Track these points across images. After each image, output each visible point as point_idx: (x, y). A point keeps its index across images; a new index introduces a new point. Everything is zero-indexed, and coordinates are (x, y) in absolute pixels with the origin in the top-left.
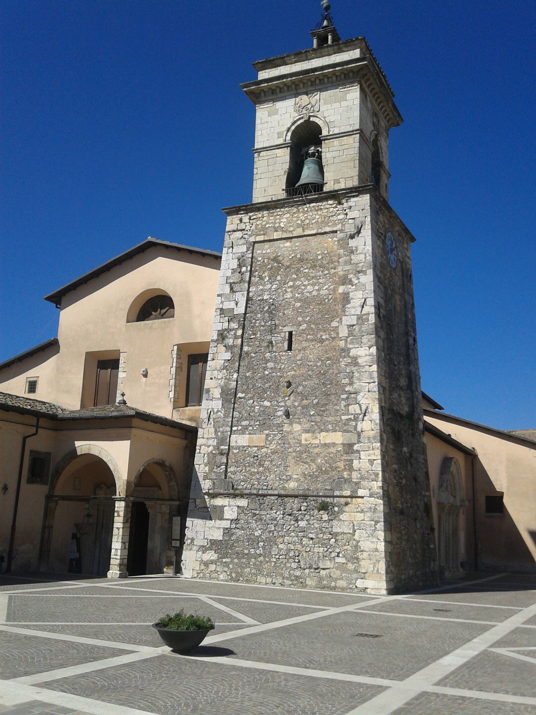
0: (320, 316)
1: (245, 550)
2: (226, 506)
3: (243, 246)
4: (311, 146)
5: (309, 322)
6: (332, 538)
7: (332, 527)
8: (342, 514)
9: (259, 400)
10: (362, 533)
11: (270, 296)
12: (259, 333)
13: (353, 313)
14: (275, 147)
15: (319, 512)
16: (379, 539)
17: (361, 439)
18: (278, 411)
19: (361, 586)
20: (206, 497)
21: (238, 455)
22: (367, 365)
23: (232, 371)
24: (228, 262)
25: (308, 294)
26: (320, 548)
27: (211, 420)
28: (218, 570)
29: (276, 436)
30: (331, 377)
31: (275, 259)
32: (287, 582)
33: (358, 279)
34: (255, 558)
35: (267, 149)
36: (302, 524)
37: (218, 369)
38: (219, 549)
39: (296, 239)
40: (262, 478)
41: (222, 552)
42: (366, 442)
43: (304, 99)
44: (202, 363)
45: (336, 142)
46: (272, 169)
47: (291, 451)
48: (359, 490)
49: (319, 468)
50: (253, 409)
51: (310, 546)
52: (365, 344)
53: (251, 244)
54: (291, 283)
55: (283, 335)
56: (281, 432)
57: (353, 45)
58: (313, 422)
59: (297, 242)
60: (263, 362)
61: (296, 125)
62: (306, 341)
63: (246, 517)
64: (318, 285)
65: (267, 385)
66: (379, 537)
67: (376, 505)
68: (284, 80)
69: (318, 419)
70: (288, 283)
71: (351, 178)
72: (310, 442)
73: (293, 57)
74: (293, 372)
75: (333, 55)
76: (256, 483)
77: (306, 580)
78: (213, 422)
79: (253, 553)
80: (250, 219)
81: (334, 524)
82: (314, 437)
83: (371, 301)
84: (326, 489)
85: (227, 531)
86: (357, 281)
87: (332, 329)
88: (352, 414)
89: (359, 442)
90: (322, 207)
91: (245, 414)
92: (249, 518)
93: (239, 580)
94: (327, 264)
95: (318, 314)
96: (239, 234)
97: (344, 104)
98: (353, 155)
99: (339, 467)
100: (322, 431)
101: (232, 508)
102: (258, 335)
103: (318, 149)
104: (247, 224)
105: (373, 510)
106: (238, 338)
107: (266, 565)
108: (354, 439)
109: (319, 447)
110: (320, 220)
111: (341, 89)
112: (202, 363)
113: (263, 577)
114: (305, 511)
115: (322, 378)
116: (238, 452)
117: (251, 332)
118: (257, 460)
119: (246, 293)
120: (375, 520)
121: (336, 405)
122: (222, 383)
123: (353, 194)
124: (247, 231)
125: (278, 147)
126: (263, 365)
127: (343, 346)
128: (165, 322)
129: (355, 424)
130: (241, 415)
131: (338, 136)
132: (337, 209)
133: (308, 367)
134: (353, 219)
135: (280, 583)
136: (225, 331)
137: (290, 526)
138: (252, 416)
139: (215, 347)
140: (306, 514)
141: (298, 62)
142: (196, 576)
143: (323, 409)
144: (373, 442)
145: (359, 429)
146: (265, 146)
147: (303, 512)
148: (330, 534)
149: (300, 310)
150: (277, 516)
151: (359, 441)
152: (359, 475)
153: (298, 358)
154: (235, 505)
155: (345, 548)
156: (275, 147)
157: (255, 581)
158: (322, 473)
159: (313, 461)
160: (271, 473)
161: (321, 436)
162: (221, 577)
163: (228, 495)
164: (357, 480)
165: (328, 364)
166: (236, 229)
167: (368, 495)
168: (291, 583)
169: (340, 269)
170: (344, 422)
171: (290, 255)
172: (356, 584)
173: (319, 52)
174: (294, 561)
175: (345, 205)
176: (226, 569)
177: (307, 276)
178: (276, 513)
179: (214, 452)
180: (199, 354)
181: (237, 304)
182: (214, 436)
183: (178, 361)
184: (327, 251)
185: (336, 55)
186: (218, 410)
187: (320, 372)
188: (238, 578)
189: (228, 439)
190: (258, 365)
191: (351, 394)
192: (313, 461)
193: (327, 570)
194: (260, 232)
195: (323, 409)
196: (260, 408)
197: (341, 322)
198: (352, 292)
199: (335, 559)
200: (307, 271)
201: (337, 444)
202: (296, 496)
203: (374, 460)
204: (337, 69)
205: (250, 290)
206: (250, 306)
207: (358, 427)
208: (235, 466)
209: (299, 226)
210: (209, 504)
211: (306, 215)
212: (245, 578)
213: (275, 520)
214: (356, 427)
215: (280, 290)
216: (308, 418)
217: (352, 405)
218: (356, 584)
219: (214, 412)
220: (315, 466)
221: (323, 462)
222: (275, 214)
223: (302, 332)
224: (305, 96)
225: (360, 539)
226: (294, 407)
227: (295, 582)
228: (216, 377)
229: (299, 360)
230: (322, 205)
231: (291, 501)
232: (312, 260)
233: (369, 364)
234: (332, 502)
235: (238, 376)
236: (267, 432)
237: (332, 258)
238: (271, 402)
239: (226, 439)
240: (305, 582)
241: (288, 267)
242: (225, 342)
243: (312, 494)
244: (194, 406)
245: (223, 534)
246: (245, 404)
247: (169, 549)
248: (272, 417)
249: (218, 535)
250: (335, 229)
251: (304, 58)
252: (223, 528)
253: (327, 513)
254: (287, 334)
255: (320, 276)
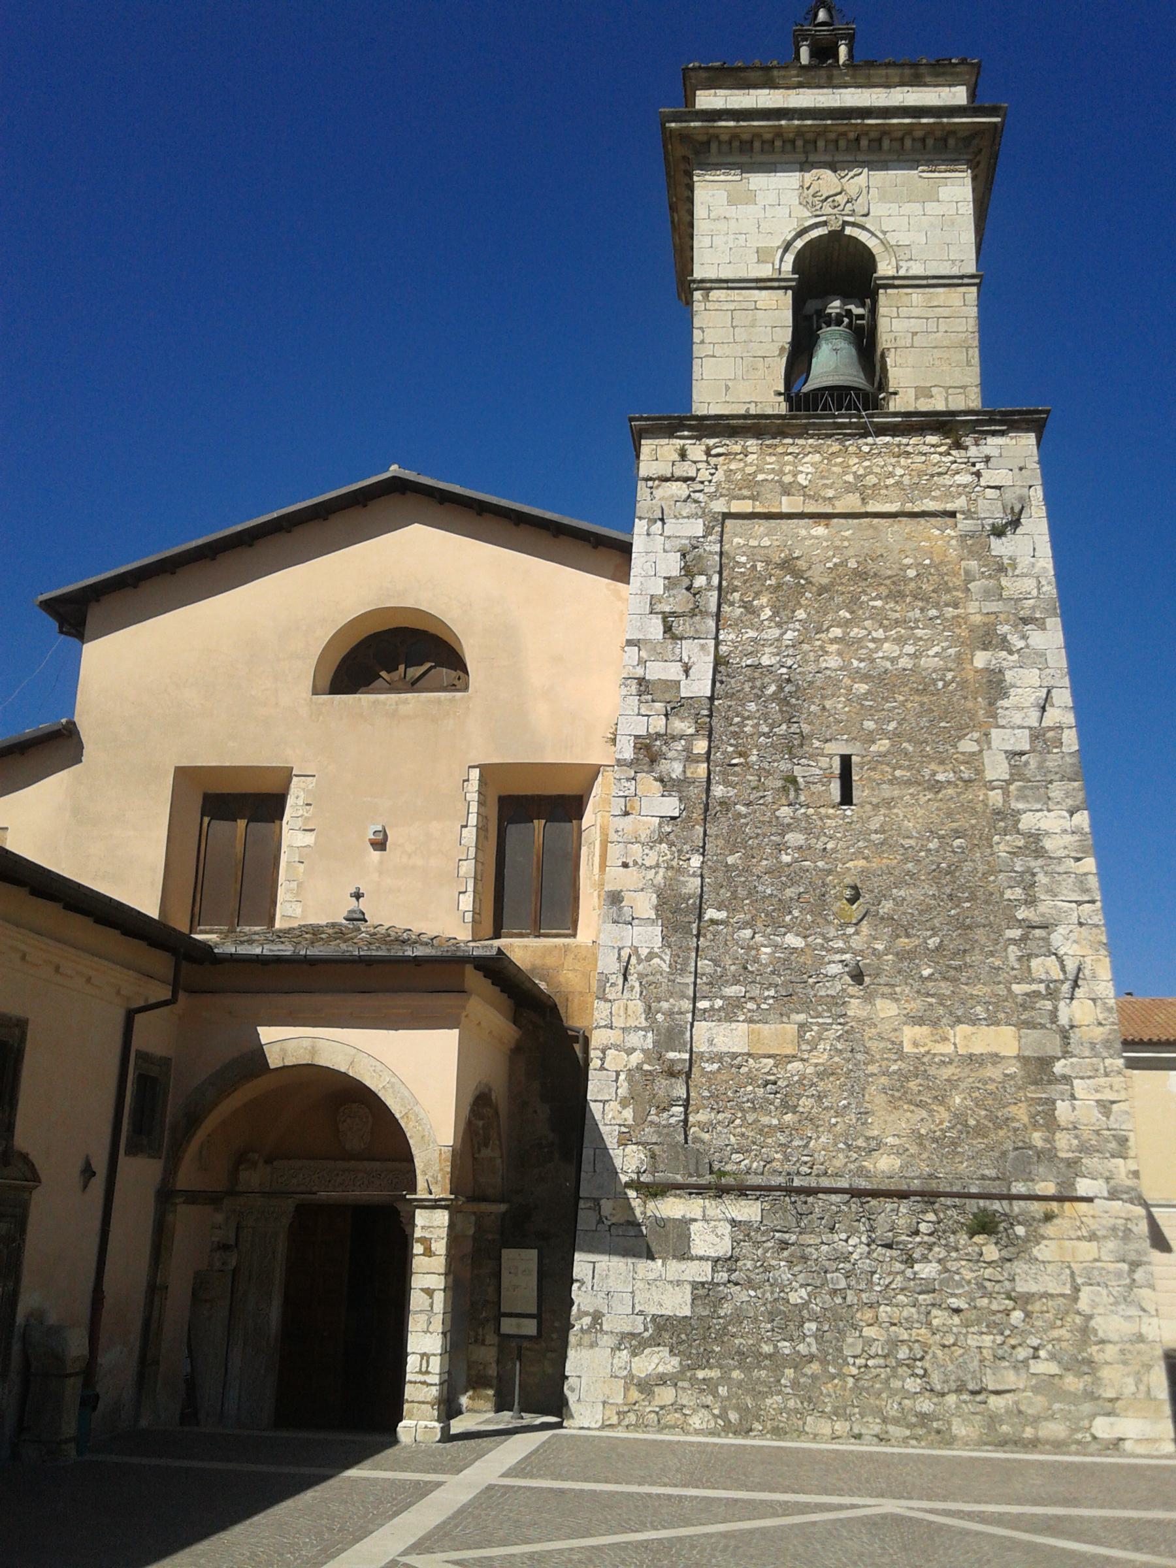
0: (924, 722)
1: (763, 1345)
2: (695, 1220)
3: (693, 520)
4: (831, 297)
5: (896, 736)
6: (1014, 1309)
7: (1014, 1280)
8: (1038, 1244)
9: (769, 930)
10: (1099, 1294)
11: (778, 658)
12: (755, 752)
13: (1019, 722)
14: (753, 285)
15: (971, 1238)
16: (1144, 1310)
17: (1072, 1045)
18: (829, 963)
19: (1106, 1436)
20: (632, 1194)
21: (719, 1077)
22: (1068, 856)
23: (686, 847)
24: (652, 557)
25: (888, 665)
26: (984, 1337)
27: (633, 979)
28: (685, 1402)
29: (827, 1030)
30: (969, 881)
31: (787, 565)
32: (895, 1431)
33: (1024, 637)
34: (795, 1368)
35: (730, 285)
36: (927, 1270)
37: (642, 840)
38: (682, 1342)
39: (842, 521)
40: (796, 1143)
41: (694, 1351)
42: (1087, 1054)
43: (826, 180)
44: (543, 821)
45: (917, 296)
46: (744, 337)
47: (876, 1071)
48: (1078, 1179)
49: (959, 1118)
50: (753, 952)
51: (955, 1330)
52: (1058, 803)
53: (716, 520)
54: (837, 632)
55: (824, 762)
56: (842, 1020)
57: (952, 74)
58: (932, 996)
59: (848, 529)
60: (774, 830)
61: (807, 238)
62: (891, 782)
63: (760, 1252)
64: (914, 644)
65: (790, 892)
66: (1144, 1305)
67: (1127, 1219)
68: (783, 122)
69: (945, 988)
70: (828, 630)
71: (962, 391)
72: (926, 1049)
73: (794, 72)
74: (861, 863)
75: (898, 89)
76: (778, 1156)
77: (949, 1423)
78: (637, 984)
79: (787, 1351)
80: (708, 453)
81: (1018, 1271)
82: (937, 1037)
83: (1063, 696)
84: (983, 1177)
85: (701, 1292)
86: (1021, 644)
87: (961, 757)
88: (1042, 981)
89: (1066, 1054)
90: (909, 449)
91: (733, 968)
92: (768, 1255)
93: (751, 1430)
94: (933, 591)
95: (919, 715)
96: (678, 489)
97: (931, 207)
98: (964, 335)
99: (1013, 1119)
100: (959, 1021)
101: (715, 1227)
102: (754, 758)
103: (849, 307)
104: (700, 465)
105: (1120, 1234)
106: (698, 762)
107: (830, 1385)
108: (1053, 1046)
109: (955, 1064)
110: (906, 480)
111: (923, 171)
112: (543, 821)
113: (823, 1420)
114: (931, 1234)
115: (944, 882)
116: (719, 1068)
117: (730, 749)
118: (776, 1093)
119: (711, 643)
120: (1129, 1258)
121: (993, 956)
122: (659, 879)
123: (993, 428)
124: (702, 482)
125: (761, 284)
126: (773, 838)
127: (1000, 805)
128: (439, 702)
129: (1050, 1008)
130: (719, 969)
131: (924, 282)
132: (951, 458)
133: (902, 851)
134: (998, 488)
135: (877, 1436)
136: (656, 740)
137: (891, 1278)
138: (752, 972)
139: (628, 780)
140: (935, 1243)
141: (803, 87)
142: (614, 1420)
143: (957, 963)
144: (1105, 1054)
145: (1063, 1020)
146: (723, 276)
147: (926, 1238)
148: (1009, 1298)
149: (867, 703)
150: (851, 1249)
151: (1067, 1052)
152: (1075, 1142)
153: (875, 824)
154: (721, 1216)
155: (1055, 1333)
156: (753, 285)
157: (801, 1433)
158: (968, 1132)
159: (941, 1100)
160: (820, 1129)
161: (957, 1034)
162: (696, 1421)
163: (699, 1190)
164: (1070, 1155)
165: (959, 847)
166: (669, 475)
167: (1106, 1194)
168: (908, 1433)
169: (973, 607)
170: (1019, 1000)
171: (829, 559)
172: (1093, 1430)
173: (809, 78)
174: (910, 1372)
175: (973, 451)
176: (709, 1400)
177: (880, 618)
178: (846, 1241)
179: (646, 1067)
180: (533, 797)
181: (687, 672)
182: (644, 1024)
183: (483, 809)
184: (931, 559)
185: (906, 89)
186: (650, 953)
187: (938, 867)
188: (746, 1426)
189: (688, 1034)
190: (761, 838)
191: (1034, 927)
192: (941, 1100)
193: (1008, 1396)
194: (740, 489)
195: (957, 963)
196: (775, 952)
197: (989, 743)
198: (1010, 669)
199: (1028, 1367)
200: (879, 603)
201: (1004, 1057)
202: (903, 1195)
203: (1113, 1102)
204: (924, 121)
205: (721, 637)
206: (724, 679)
207: (1059, 1013)
208: (712, 1108)
209: (849, 488)
210: (644, 1213)
211: (867, 463)
212: (769, 1424)
213: (846, 1259)
214: (1054, 1015)
215: (806, 647)
216: (916, 985)
217: (1037, 956)
218: (1093, 1430)
219: (638, 956)
220: (945, 1115)
221: (969, 1103)
222: (780, 450)
223: (880, 759)
224: (829, 172)
225: (1095, 1311)
226: (874, 954)
227: (920, 1431)
228: (640, 862)
229: (876, 832)
230: (908, 445)
231: (889, 1207)
232: (890, 577)
233: (1074, 854)
234: (1008, 1211)
235: (703, 863)
236: (801, 1017)
237: (946, 578)
238: (805, 937)
239: (683, 1033)
240: (949, 1429)
241: (823, 589)
242: (657, 769)
243: (948, 1190)
244: (521, 936)
245: (693, 1300)
246: (729, 938)
247: (476, 1341)
248: (810, 977)
249: (678, 1304)
250: (950, 507)
251: (823, 81)
252: (690, 1282)
253: (995, 1241)
254: (837, 762)
255: (917, 621)
